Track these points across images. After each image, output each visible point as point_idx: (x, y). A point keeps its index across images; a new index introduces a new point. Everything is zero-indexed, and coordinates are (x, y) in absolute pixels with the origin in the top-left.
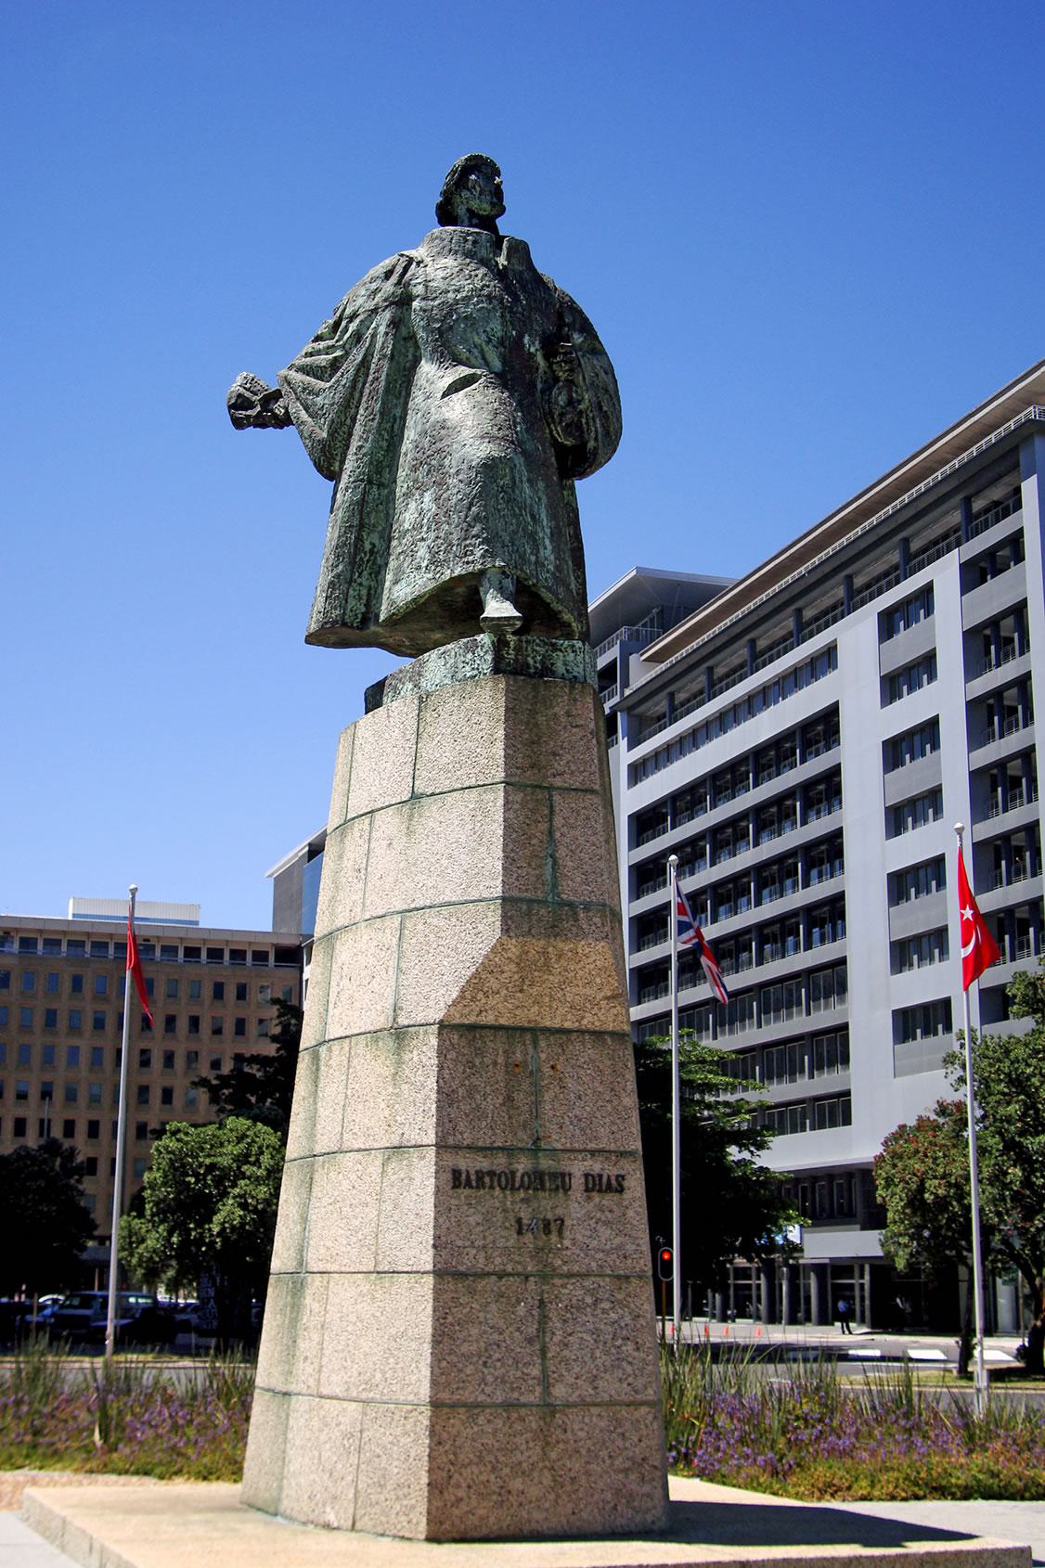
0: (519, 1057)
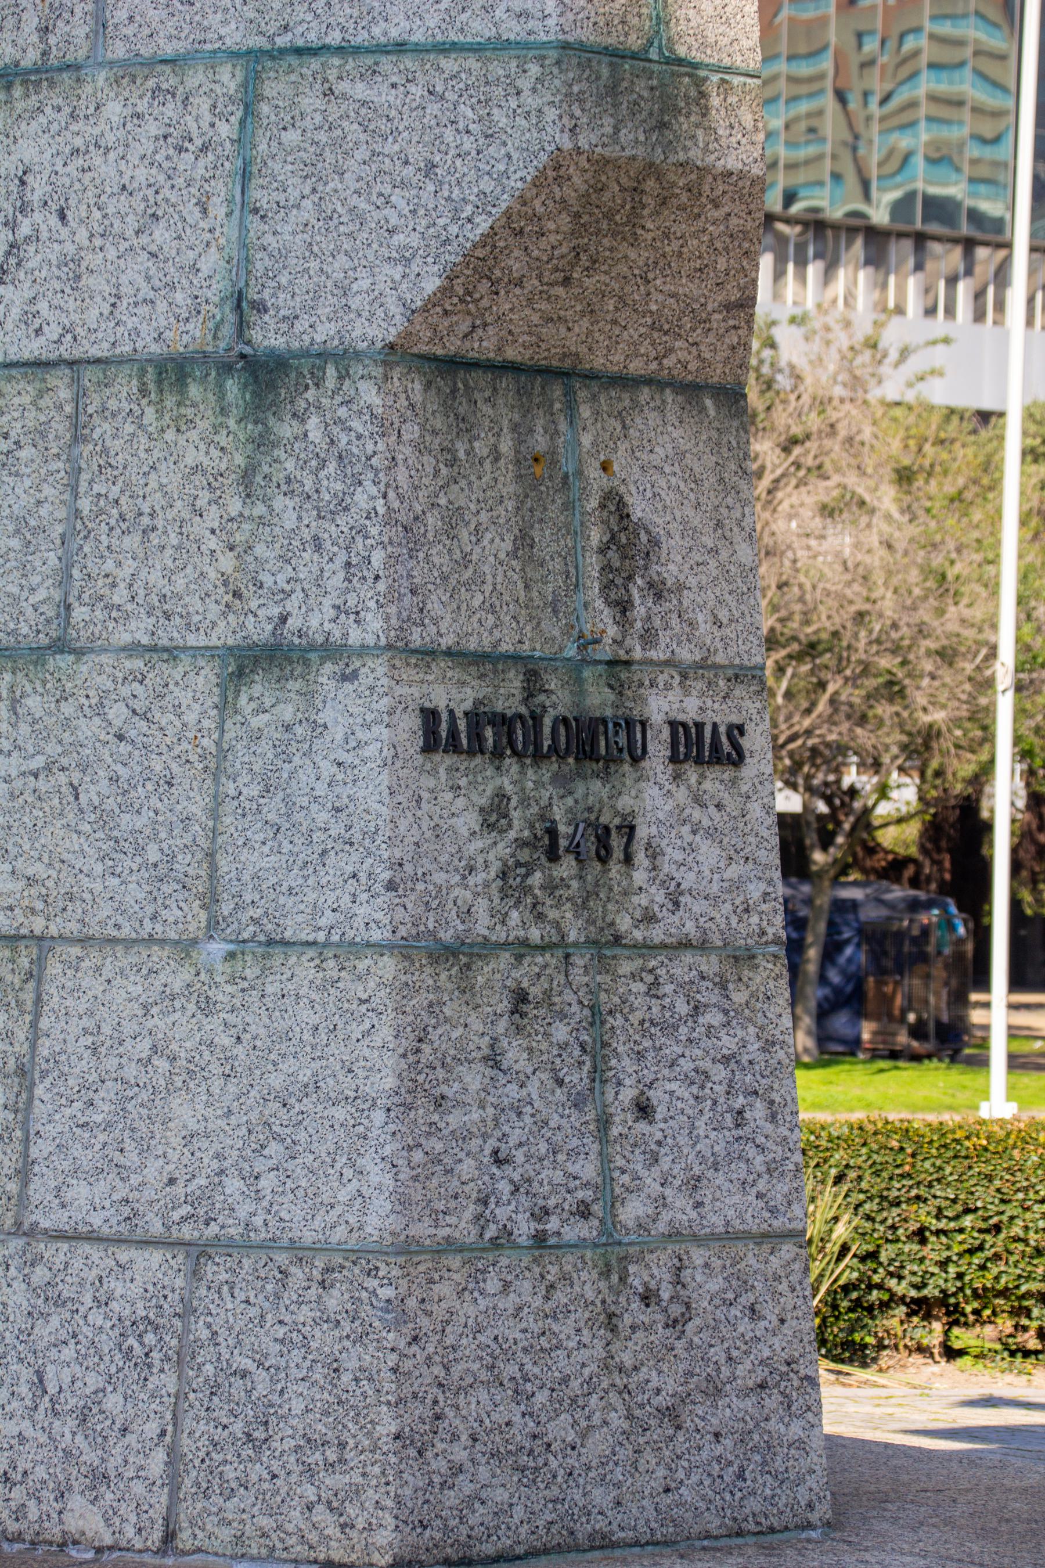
0: (540, 442)
